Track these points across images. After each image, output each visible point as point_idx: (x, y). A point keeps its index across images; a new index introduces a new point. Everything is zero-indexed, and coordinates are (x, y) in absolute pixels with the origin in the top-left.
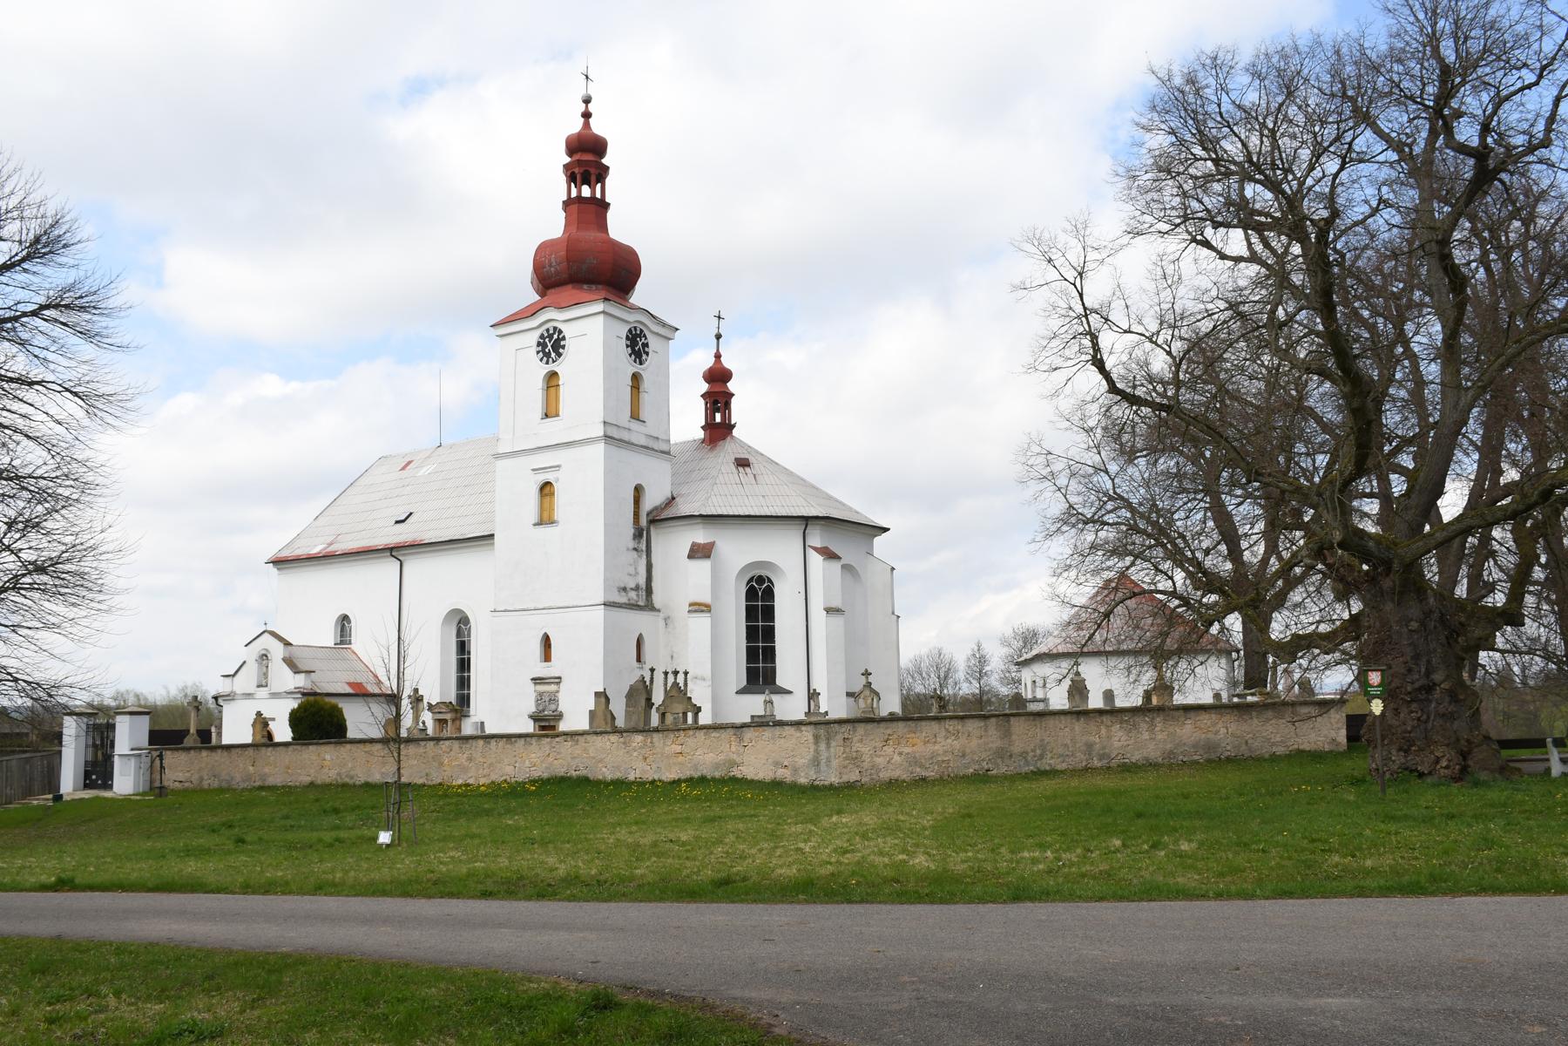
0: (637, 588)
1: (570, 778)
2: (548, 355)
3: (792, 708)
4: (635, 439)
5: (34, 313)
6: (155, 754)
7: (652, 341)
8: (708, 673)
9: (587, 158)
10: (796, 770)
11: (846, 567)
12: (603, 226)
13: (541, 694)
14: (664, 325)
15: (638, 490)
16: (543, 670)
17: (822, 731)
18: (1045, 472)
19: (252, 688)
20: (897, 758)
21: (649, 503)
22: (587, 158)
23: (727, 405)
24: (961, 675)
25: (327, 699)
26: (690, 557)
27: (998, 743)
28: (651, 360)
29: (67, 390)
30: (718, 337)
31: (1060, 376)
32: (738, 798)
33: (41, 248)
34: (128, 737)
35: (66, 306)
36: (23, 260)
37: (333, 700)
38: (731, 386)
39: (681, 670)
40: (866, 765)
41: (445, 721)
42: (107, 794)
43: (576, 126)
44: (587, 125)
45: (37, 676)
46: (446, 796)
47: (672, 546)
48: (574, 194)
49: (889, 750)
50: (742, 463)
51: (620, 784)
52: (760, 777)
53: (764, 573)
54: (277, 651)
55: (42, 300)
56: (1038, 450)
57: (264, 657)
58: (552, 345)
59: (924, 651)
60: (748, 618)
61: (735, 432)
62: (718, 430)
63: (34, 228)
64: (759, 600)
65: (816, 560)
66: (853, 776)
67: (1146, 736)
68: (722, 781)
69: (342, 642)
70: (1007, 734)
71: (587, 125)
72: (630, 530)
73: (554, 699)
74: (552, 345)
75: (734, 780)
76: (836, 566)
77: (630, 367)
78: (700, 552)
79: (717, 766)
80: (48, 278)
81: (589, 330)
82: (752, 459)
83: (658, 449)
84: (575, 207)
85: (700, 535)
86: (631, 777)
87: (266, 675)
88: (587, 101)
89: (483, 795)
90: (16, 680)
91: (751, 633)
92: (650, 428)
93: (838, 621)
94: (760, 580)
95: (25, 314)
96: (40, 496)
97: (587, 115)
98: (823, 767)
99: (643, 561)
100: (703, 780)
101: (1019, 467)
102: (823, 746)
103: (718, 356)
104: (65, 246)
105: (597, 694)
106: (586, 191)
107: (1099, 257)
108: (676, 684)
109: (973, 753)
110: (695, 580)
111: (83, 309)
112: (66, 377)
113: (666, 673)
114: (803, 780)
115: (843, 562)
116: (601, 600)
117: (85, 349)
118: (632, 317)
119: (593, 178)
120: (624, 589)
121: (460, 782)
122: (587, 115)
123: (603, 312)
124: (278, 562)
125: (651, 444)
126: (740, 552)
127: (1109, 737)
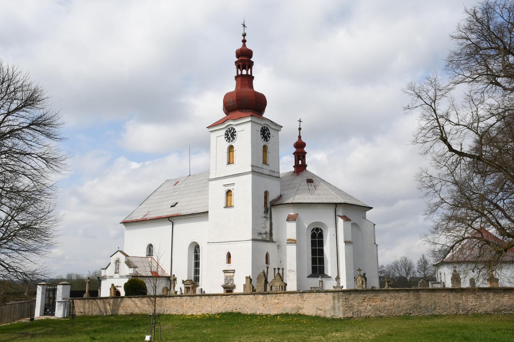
0: (266, 233)
1: (234, 313)
2: (229, 139)
3: (330, 285)
4: (265, 172)
5: (26, 127)
6: (71, 301)
7: (272, 132)
8: (295, 268)
9: (244, 59)
10: (325, 312)
11: (354, 224)
12: (251, 86)
13: (227, 277)
14: (276, 125)
15: (266, 193)
16: (228, 267)
17: (336, 295)
18: (429, 184)
19: (112, 274)
20: (369, 307)
21: (271, 198)
22: (244, 59)
23: (304, 157)
24: (415, 269)
25: (139, 278)
26: (287, 220)
27: (414, 302)
28: (271, 140)
29: (39, 157)
30: (300, 129)
31: (428, 145)
32: (300, 323)
33: (31, 101)
34: (61, 293)
35: (39, 124)
36: (23, 107)
37: (141, 279)
38: (305, 149)
39: (281, 268)
40: (355, 310)
41: (189, 288)
42: (52, 318)
43: (240, 46)
44: (244, 45)
45: (24, 270)
46: (183, 319)
47: (280, 215)
48: (240, 73)
49: (365, 304)
50: (310, 181)
51: (253, 316)
52: (310, 314)
53: (319, 227)
54: (123, 258)
55: (29, 122)
56: (426, 175)
57: (117, 261)
58: (231, 135)
59: (399, 259)
60: (312, 246)
61: (307, 168)
62: (300, 167)
63: (28, 94)
64: (317, 238)
65: (340, 221)
66: (350, 315)
67: (485, 301)
68: (295, 315)
69: (149, 255)
70: (418, 298)
71: (244, 45)
72: (263, 210)
73: (232, 279)
74: (231, 135)
75: (300, 315)
76: (349, 224)
77: (262, 143)
78: (290, 219)
79: (293, 309)
80: (33, 113)
81: (245, 129)
82: (314, 179)
83: (275, 176)
84: (240, 79)
85: (292, 212)
86: (258, 313)
87: (118, 268)
88: (244, 35)
89: (198, 319)
90: (16, 271)
91: (314, 252)
92: (271, 167)
93: (351, 247)
94: (317, 229)
95: (24, 127)
96: (26, 199)
97: (244, 41)
98: (337, 310)
99: (269, 222)
100: (287, 315)
101: (418, 183)
102: (336, 301)
103: (300, 137)
104: (38, 101)
105: (247, 278)
106: (244, 72)
107: (441, 93)
108: (279, 274)
109: (403, 306)
110: (290, 230)
111: (45, 125)
112: (38, 152)
113: (275, 269)
114: (328, 316)
115: (352, 222)
116: (251, 238)
117: (47, 141)
118: (263, 122)
119: (247, 67)
120: (261, 234)
121: (190, 314)
122: (244, 41)
123: (251, 121)
124: (125, 223)
125: (271, 174)
126: (309, 219)
127: (467, 301)
